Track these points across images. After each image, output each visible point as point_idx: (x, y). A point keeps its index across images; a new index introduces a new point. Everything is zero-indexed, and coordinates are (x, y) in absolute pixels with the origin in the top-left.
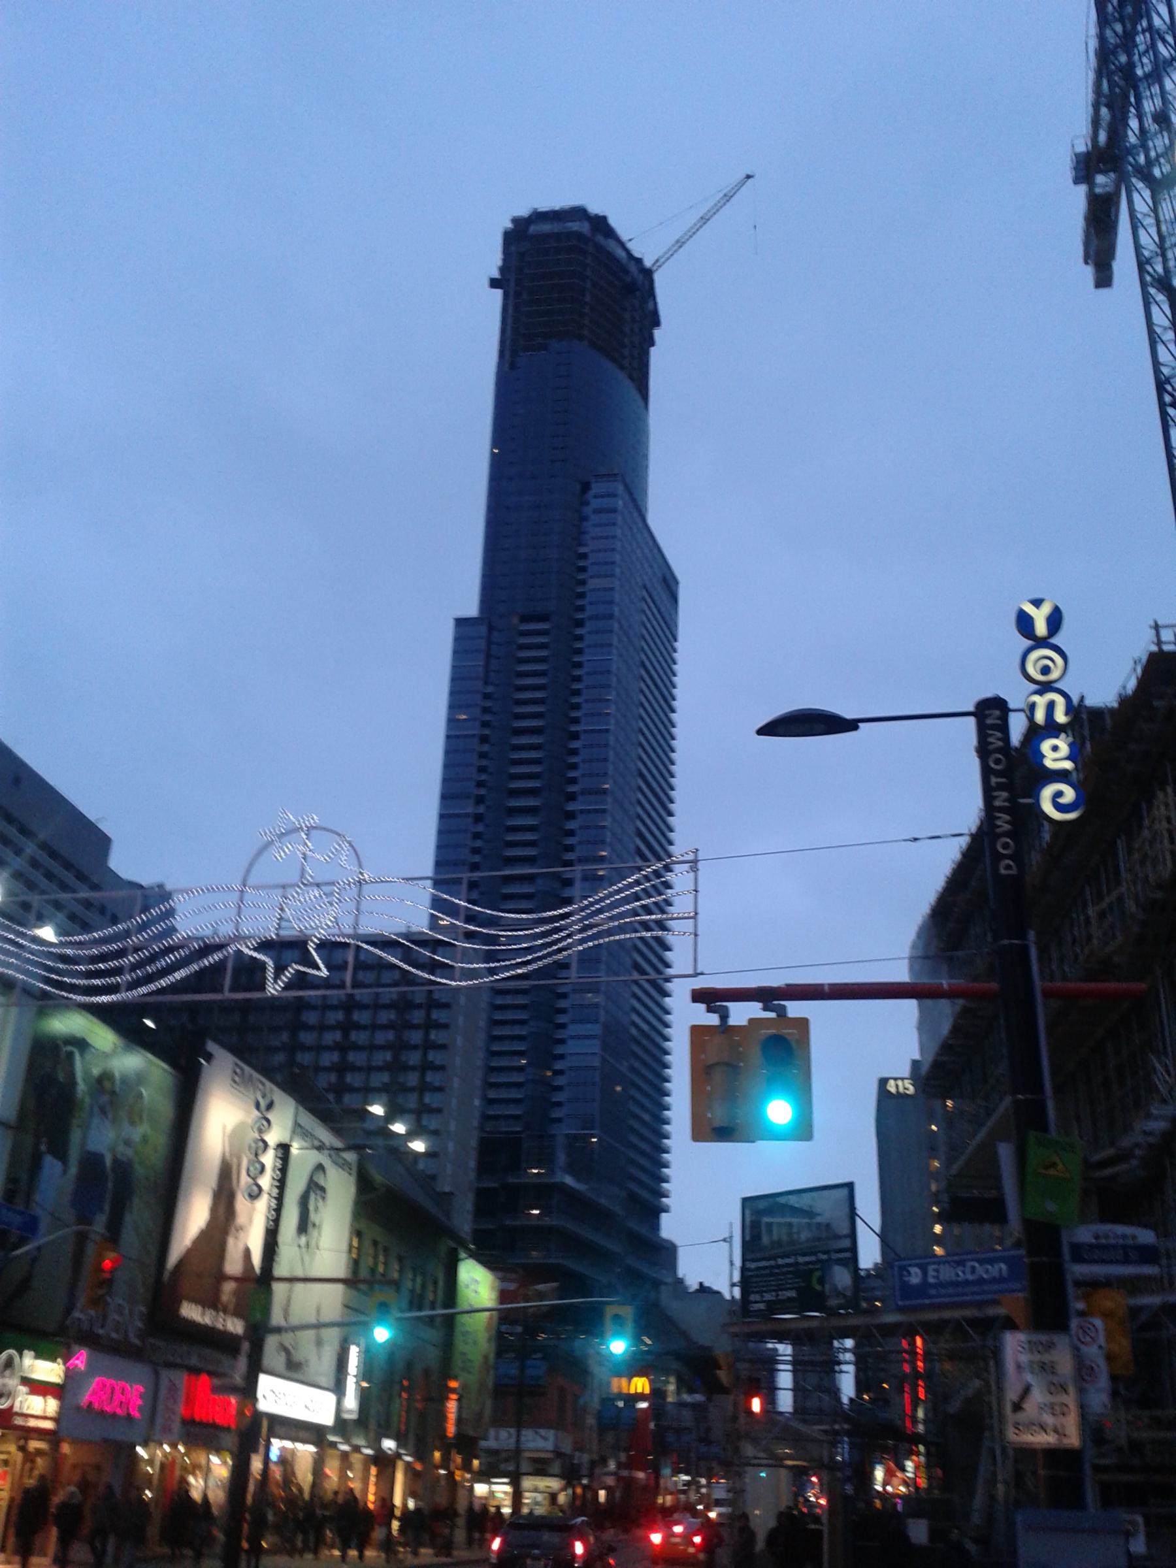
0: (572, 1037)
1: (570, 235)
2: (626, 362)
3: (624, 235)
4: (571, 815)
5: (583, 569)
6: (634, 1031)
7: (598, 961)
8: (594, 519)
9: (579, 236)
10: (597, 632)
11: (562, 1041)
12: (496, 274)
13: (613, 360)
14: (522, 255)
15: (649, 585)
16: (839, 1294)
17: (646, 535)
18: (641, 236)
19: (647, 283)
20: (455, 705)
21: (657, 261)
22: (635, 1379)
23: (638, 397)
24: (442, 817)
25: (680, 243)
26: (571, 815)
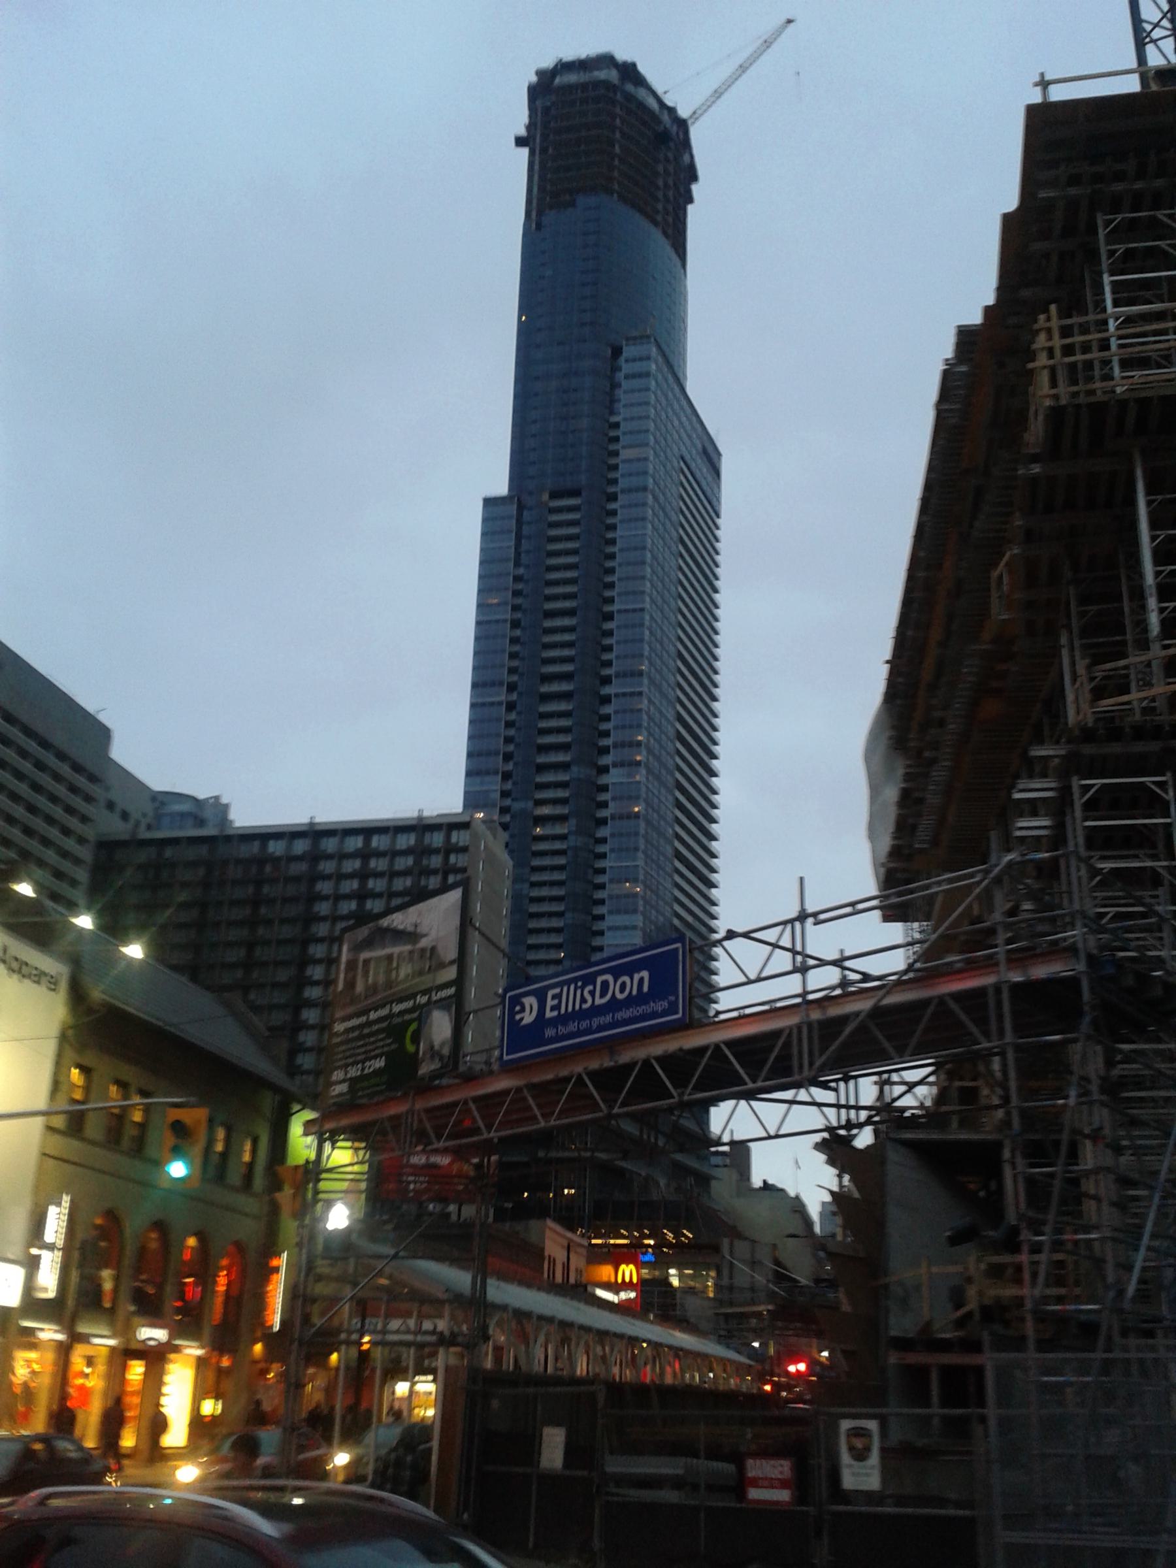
0: (610, 928)
1: (597, 84)
2: (659, 218)
3: (659, 89)
4: (606, 700)
5: (616, 439)
6: (676, 922)
7: (636, 849)
8: (625, 385)
9: (607, 84)
10: (630, 506)
11: (601, 933)
12: (522, 132)
13: (641, 211)
14: (546, 111)
15: (687, 458)
16: (433, 1053)
17: (684, 403)
18: (675, 83)
20: (484, 590)
21: (694, 113)
22: (623, 1267)
23: (669, 251)
24: (473, 706)
26: (606, 700)
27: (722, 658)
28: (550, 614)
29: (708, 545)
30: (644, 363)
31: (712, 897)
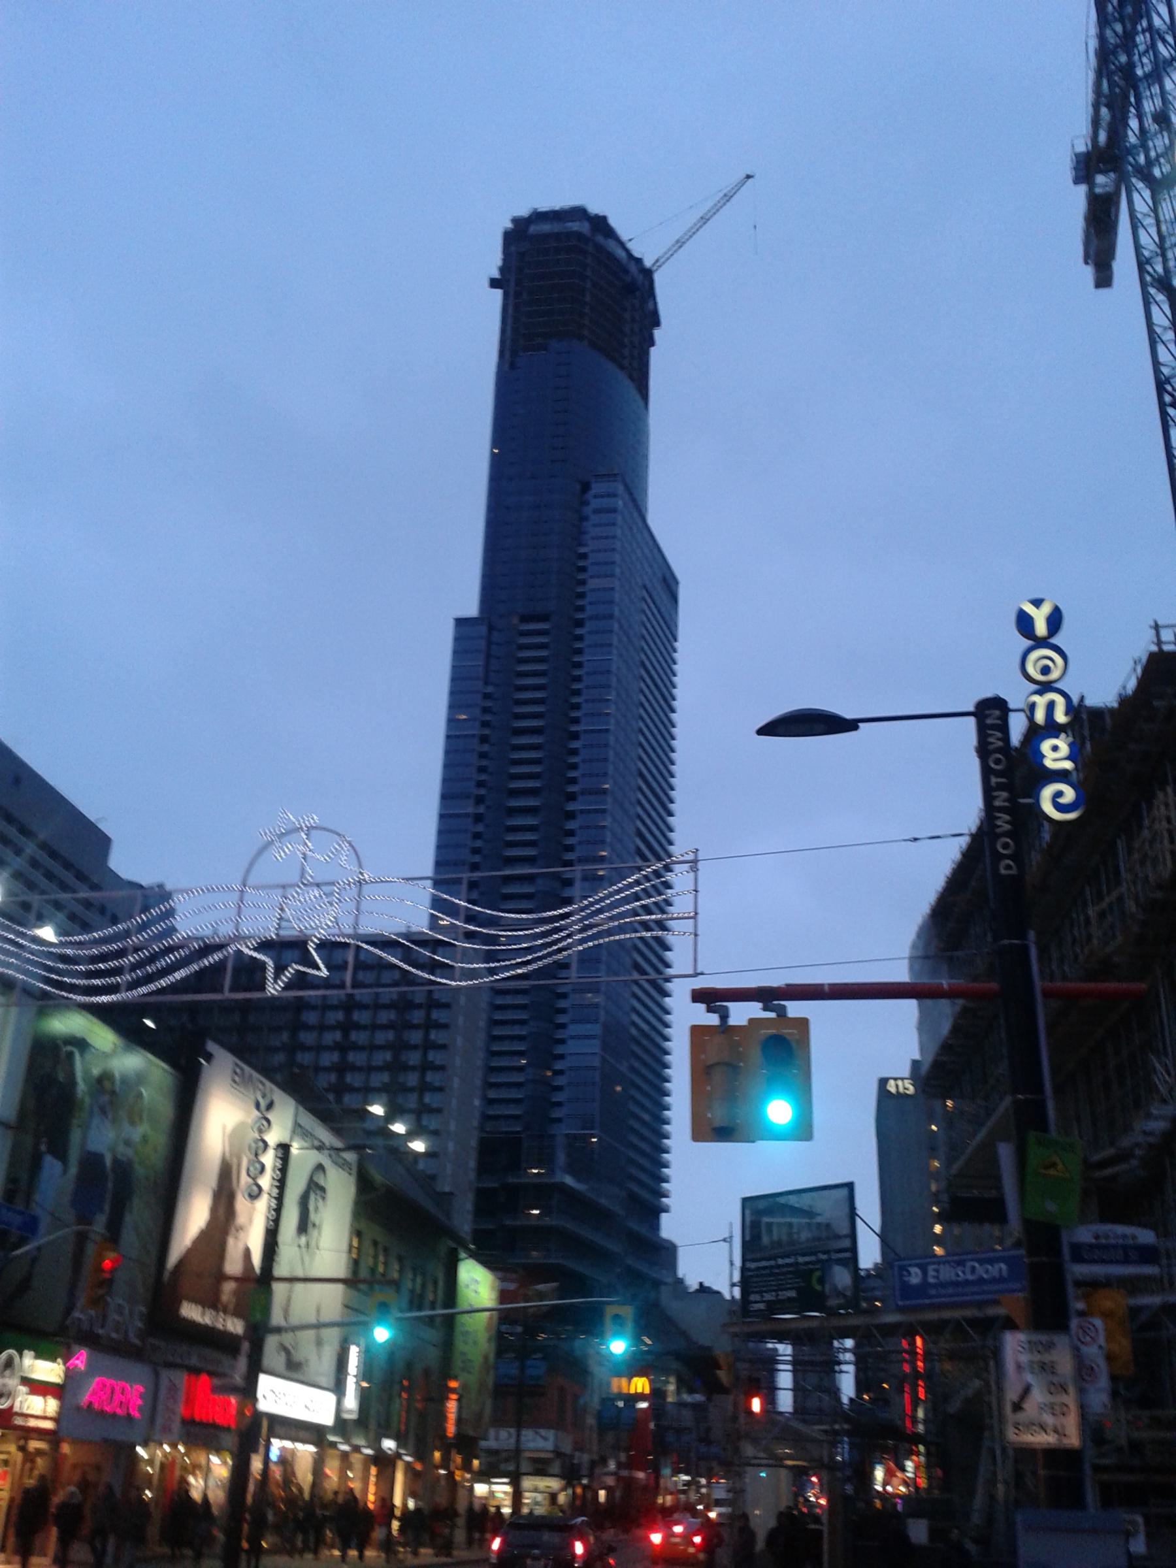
0: (572, 1037)
1: (570, 235)
2: (626, 362)
3: (624, 235)
4: (571, 815)
5: (583, 569)
6: (634, 1031)
7: (598, 961)
8: (594, 519)
9: (579, 236)
10: (597, 632)
11: (562, 1041)
12: (496, 274)
13: (613, 360)
14: (522, 255)
15: (649, 585)
16: (839, 1294)
17: (646, 535)
18: (641, 236)
19: (647, 283)
20: (455, 705)
21: (657, 261)
22: (635, 1379)
23: (638, 397)
24: (442, 817)
25: (680, 243)
26: (571, 815)
27: (677, 788)
28: (514, 793)
29: (661, 767)
30: (612, 515)
31: (666, 959)
